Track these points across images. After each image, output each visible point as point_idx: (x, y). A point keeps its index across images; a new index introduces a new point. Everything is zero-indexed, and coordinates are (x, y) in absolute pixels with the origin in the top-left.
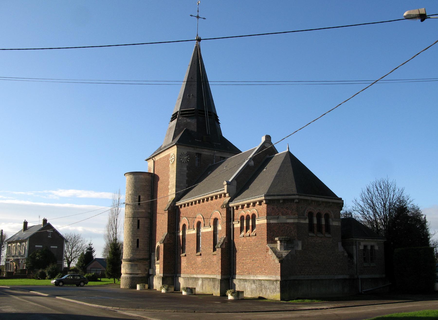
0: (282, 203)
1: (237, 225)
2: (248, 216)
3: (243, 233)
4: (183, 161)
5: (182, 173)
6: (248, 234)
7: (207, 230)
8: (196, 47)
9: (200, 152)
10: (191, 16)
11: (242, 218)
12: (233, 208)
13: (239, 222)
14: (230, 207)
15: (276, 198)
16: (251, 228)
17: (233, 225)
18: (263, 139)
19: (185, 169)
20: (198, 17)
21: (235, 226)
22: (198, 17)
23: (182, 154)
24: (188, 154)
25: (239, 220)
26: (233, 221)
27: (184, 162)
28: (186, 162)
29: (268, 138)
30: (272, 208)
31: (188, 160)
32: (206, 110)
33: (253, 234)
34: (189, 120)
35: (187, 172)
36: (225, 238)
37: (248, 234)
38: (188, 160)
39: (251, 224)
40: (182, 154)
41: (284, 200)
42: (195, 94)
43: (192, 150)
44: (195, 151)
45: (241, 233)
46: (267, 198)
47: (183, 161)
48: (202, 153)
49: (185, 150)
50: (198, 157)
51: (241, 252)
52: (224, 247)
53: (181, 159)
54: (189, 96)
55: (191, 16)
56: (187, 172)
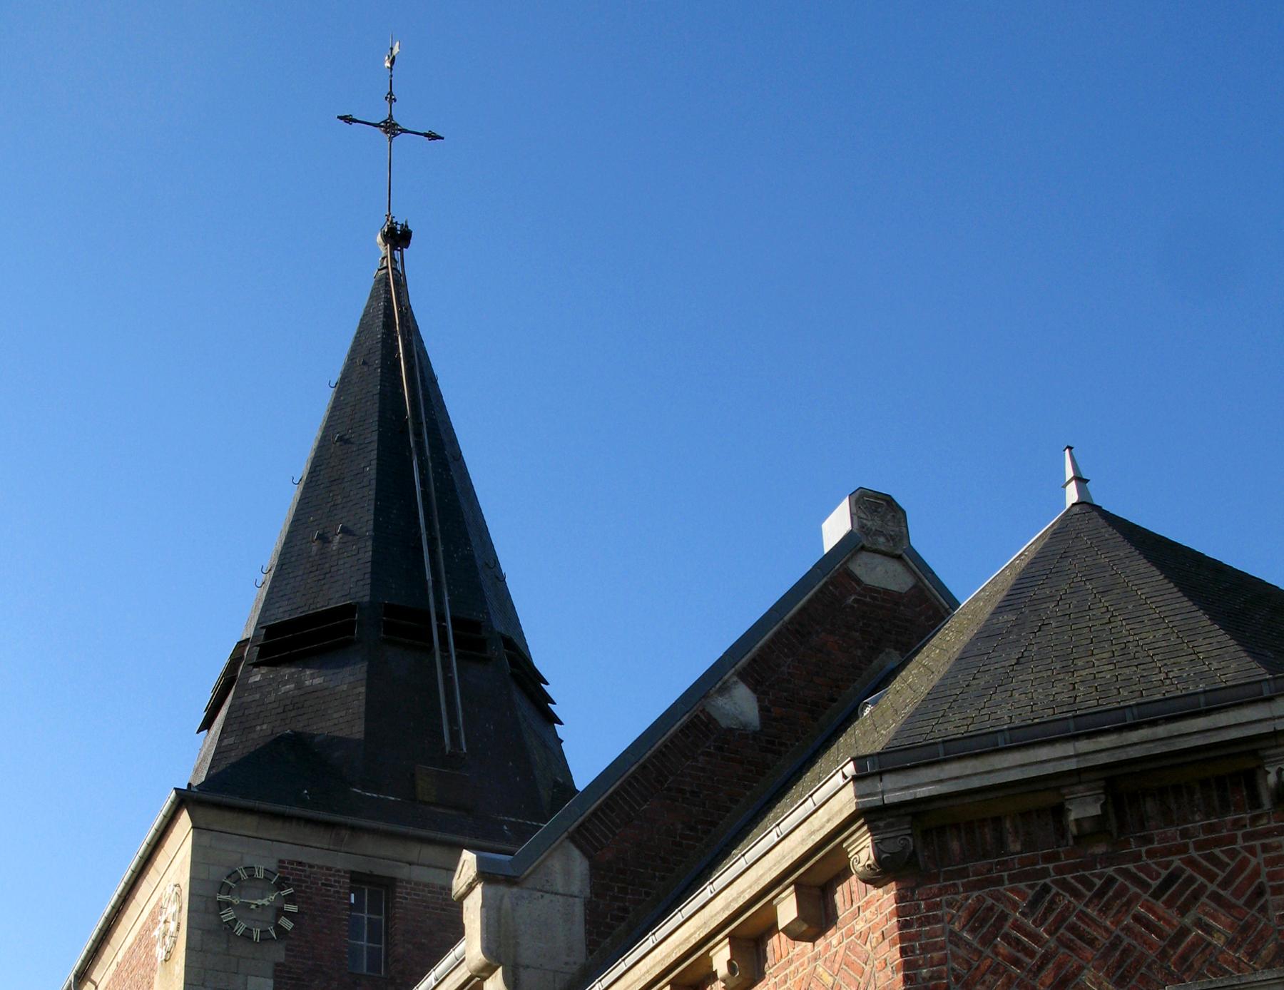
0: (1098, 828)
4: (240, 929)
8: (382, 282)
9: (381, 869)
10: (348, 119)
15: (1009, 767)
18: (837, 525)
20: (390, 128)
22: (390, 128)
23: (232, 874)
27: (247, 936)
28: (265, 937)
29: (879, 514)
30: (977, 919)
31: (287, 924)
32: (441, 607)
34: (312, 678)
38: (287, 924)
40: (232, 874)
41: (1127, 788)
42: (365, 521)
43: (323, 855)
44: (342, 862)
46: (895, 790)
47: (240, 929)
48: (403, 872)
49: (262, 850)
50: (374, 909)
53: (228, 915)
54: (324, 539)
55: (348, 119)
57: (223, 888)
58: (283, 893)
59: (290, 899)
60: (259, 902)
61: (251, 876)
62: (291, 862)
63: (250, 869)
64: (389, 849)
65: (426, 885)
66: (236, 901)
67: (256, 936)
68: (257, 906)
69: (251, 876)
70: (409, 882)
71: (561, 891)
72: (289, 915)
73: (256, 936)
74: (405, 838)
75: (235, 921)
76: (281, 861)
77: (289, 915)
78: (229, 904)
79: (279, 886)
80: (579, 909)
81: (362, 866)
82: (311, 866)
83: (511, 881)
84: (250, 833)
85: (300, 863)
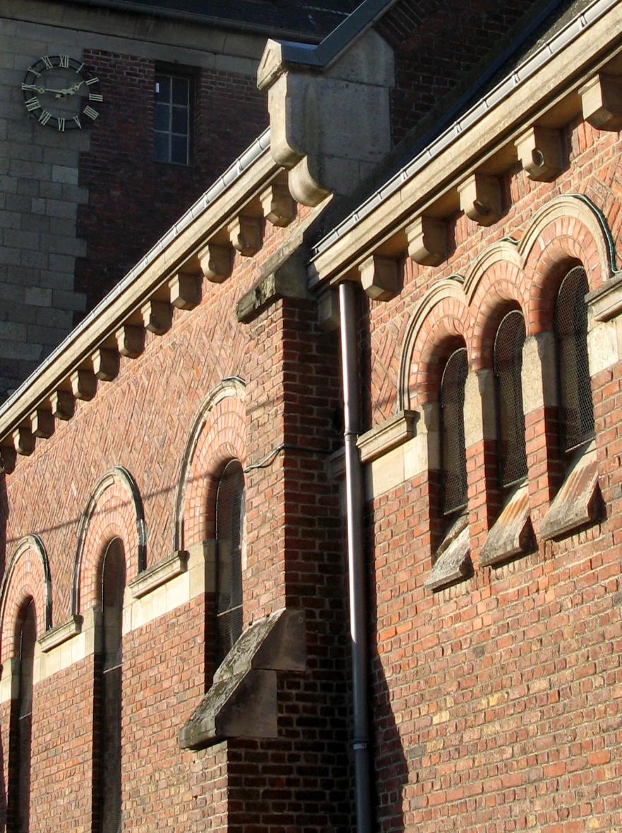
1: (398, 467)
2: (503, 316)
3: (460, 542)
4: (45, 118)
5: (38, 205)
6: (510, 526)
7: (165, 602)
11: (446, 359)
12: (353, 283)
13: (411, 418)
14: (325, 289)
16: (536, 443)
17: (363, 470)
19: (70, 175)
21: (384, 478)
24: (90, 66)
25: (417, 401)
26: (363, 423)
27: (52, 125)
31: (92, 113)
33: (573, 501)
35: (83, 196)
36: (277, 629)
37: (510, 526)
38: (92, 113)
39: (533, 398)
44: (147, 51)
45: (438, 541)
47: (45, 118)
48: (208, 61)
51: (444, 768)
52: (264, 724)
53: (34, 104)
56: (83, 196)
57: (28, 77)
58: (88, 82)
59: (95, 89)
60: (65, 92)
61: (56, 65)
62: (96, 52)
63: (55, 59)
64: (193, 38)
65: (231, 74)
66: (41, 90)
67: (61, 125)
68: (62, 95)
69: (56, 65)
70: (214, 71)
71: (366, 80)
72: (95, 105)
73: (61, 125)
74: (209, 27)
75: (40, 110)
76: (86, 51)
77: (95, 105)
78: (34, 93)
79: (84, 76)
80: (383, 99)
81: (166, 55)
82: (116, 56)
83: (316, 70)
84: (55, 23)
85: (105, 53)
